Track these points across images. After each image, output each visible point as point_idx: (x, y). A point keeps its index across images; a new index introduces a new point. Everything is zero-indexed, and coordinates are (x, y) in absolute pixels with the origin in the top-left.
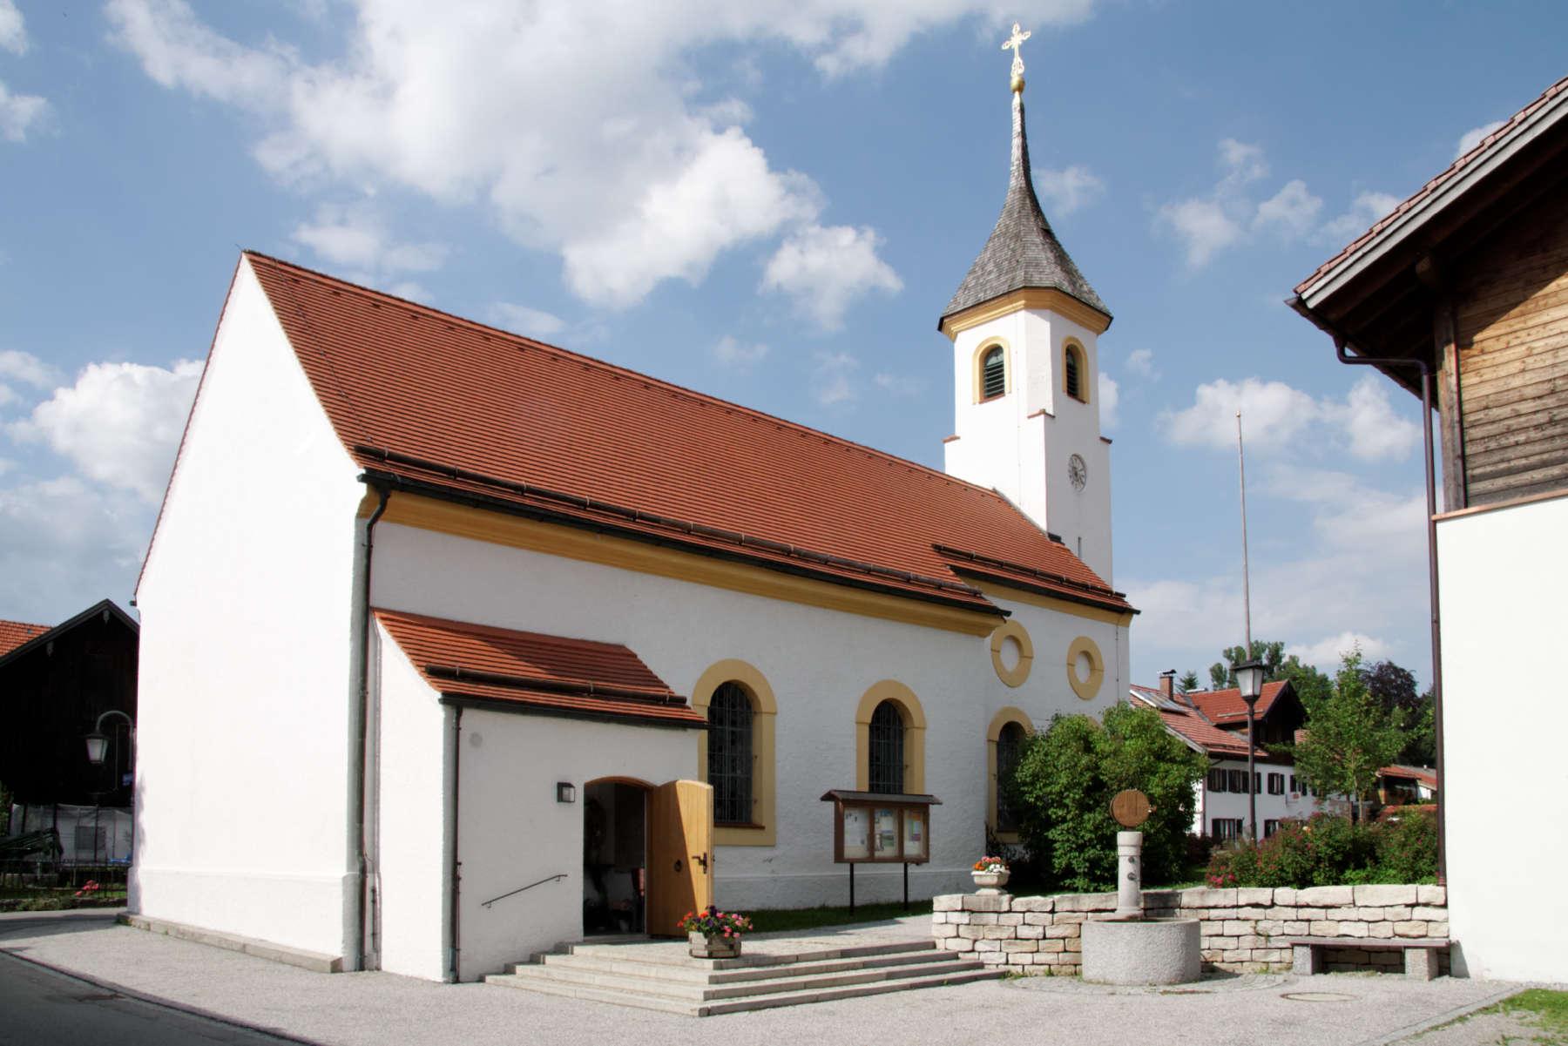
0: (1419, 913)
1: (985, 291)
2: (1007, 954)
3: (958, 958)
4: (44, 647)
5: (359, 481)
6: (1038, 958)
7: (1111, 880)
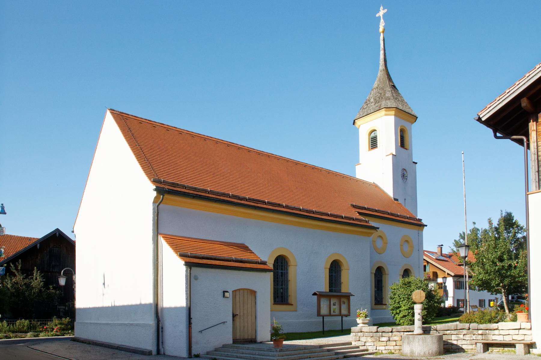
0: (521, 332)
1: (370, 110)
2: (376, 346)
3: (359, 348)
4: (36, 246)
5: (154, 191)
6: (387, 348)
7: (412, 323)
